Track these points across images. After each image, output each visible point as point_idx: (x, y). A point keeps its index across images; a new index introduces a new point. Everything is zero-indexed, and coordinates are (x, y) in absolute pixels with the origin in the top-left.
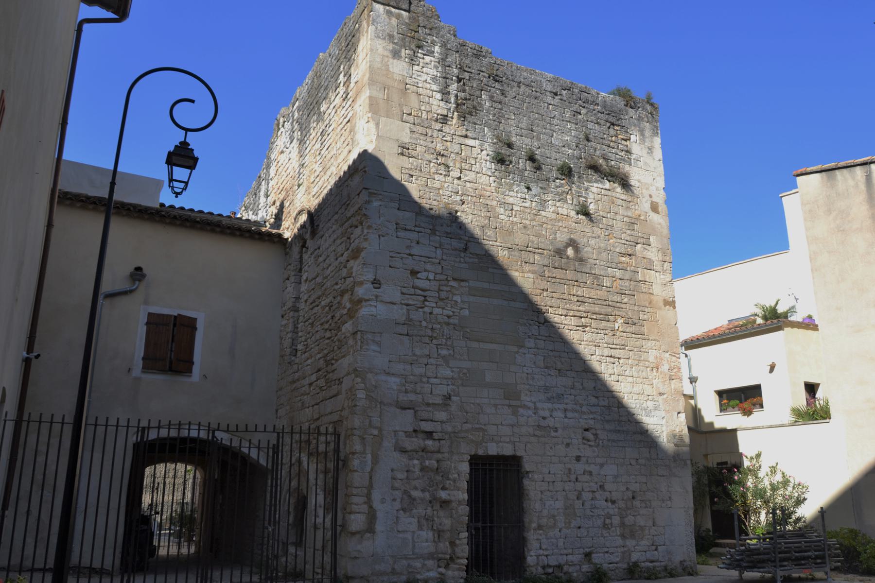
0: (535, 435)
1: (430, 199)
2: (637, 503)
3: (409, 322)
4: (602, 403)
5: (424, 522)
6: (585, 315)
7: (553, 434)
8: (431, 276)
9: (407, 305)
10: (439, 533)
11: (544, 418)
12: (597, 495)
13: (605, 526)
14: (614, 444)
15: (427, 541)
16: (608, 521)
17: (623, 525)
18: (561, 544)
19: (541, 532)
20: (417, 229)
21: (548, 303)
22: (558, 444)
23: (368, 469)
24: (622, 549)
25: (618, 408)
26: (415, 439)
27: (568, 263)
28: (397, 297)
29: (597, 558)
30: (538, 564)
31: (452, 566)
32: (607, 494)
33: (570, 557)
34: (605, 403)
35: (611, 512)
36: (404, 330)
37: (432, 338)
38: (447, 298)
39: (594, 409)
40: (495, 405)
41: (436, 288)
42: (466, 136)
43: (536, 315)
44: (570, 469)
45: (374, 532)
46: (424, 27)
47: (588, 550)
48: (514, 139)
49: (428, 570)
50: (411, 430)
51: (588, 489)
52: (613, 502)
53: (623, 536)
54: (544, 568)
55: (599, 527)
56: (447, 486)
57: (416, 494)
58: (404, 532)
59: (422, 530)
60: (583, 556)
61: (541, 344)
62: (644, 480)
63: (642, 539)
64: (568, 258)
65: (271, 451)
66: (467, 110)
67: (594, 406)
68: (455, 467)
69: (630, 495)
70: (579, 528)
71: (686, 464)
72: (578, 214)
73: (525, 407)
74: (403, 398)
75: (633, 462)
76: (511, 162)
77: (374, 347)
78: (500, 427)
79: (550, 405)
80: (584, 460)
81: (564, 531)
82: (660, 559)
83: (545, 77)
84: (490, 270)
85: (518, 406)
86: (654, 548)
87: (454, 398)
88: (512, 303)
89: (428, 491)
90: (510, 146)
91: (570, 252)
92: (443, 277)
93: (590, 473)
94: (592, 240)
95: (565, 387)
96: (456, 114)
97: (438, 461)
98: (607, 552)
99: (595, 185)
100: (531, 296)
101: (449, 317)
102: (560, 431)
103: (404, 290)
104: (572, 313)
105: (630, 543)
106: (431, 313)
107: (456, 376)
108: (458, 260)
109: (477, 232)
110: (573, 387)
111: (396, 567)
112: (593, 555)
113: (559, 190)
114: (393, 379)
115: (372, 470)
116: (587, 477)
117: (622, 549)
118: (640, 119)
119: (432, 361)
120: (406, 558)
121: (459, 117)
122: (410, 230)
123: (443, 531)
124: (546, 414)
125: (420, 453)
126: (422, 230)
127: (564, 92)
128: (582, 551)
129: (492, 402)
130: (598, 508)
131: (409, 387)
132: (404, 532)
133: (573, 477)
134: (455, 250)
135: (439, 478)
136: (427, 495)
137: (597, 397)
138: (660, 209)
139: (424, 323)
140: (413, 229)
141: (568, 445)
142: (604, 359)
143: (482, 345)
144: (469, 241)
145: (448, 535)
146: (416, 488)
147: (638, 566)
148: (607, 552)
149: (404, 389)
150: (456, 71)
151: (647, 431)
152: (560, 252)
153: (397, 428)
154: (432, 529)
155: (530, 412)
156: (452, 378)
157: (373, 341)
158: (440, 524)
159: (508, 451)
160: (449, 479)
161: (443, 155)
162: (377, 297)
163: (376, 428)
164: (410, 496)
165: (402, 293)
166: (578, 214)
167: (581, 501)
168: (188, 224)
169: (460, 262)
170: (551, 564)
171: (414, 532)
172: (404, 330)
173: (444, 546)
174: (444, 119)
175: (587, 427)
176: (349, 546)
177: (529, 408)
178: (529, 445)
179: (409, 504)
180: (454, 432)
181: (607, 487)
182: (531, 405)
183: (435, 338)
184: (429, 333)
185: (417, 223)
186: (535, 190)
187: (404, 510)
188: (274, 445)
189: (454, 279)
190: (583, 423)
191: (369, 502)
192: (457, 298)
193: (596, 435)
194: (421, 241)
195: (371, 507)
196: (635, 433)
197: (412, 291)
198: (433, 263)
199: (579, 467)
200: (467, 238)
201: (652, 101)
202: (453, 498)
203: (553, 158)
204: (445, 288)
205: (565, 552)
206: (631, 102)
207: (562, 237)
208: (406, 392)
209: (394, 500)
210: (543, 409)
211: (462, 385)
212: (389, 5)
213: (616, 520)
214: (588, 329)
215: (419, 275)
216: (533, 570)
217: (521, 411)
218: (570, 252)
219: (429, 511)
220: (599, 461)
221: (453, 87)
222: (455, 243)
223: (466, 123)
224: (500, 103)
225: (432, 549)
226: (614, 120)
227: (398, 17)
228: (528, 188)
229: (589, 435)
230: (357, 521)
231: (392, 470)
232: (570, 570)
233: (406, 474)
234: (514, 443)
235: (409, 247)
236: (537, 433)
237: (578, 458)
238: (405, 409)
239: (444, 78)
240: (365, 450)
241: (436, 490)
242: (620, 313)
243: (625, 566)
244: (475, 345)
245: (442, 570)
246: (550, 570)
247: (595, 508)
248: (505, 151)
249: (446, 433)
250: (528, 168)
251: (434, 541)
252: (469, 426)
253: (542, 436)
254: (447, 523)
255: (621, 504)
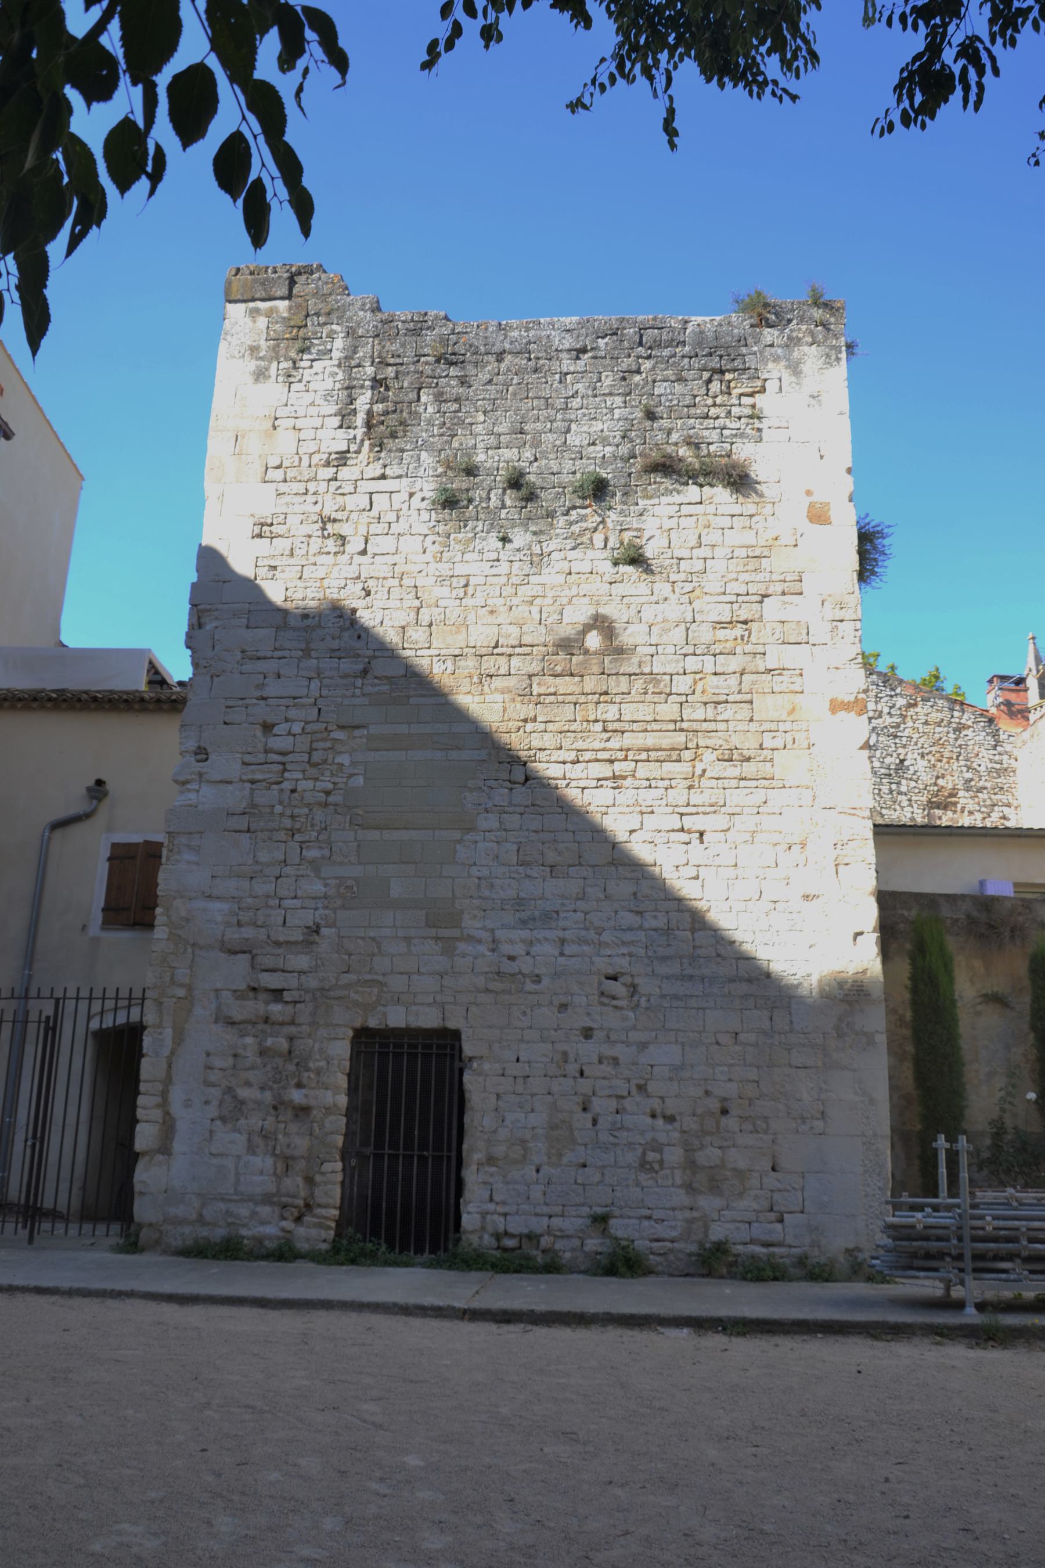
0: (487, 990)
1: (304, 599)
2: (730, 1122)
3: (251, 810)
4: (650, 922)
5: (258, 1140)
6: (620, 755)
7: (530, 986)
8: (297, 728)
9: (253, 782)
10: (287, 1162)
11: (512, 958)
12: (627, 1103)
13: (644, 1165)
14: (675, 1003)
15: (261, 1173)
16: (651, 1156)
17: (691, 1165)
18: (537, 1192)
19: (493, 1169)
20: (277, 654)
21: (536, 744)
22: (539, 1005)
23: (166, 1052)
24: (688, 1214)
25: (693, 930)
26: (251, 1003)
27: (585, 662)
28: (234, 769)
29: (619, 1228)
30: (483, 1228)
31: (307, 1219)
32: (655, 1104)
33: (557, 1222)
34: (661, 922)
35: (662, 1138)
36: (243, 823)
37: (293, 832)
38: (325, 761)
39: (628, 937)
40: (408, 939)
41: (306, 747)
42: (383, 477)
43: (511, 769)
44: (565, 1054)
45: (170, 1154)
46: (317, 314)
47: (599, 1210)
48: (480, 457)
49: (263, 1223)
50: (243, 987)
51: (607, 1092)
52: (670, 1119)
53: (689, 1188)
54: (498, 1237)
55: (629, 1167)
56: (305, 1081)
57: (244, 1093)
58: (222, 1155)
59: (254, 1154)
60: (588, 1221)
61: (513, 821)
62: (752, 1074)
63: (741, 1195)
64: (587, 652)
65: (43, 1025)
66: (385, 431)
67: (630, 929)
68: (321, 1050)
69: (714, 1105)
70: (585, 1166)
71: (871, 1042)
72: (616, 564)
73: (471, 939)
74: (234, 935)
75: (723, 1039)
76: (470, 501)
77: (188, 856)
78: (415, 977)
79: (525, 934)
80: (598, 1035)
81: (545, 1169)
82: (789, 1240)
83: (559, 327)
84: (412, 701)
85: (457, 939)
86: (772, 1216)
87: (324, 931)
88: (454, 754)
89: (271, 1089)
90: (471, 471)
91: (593, 640)
92: (321, 726)
93: (615, 1061)
94: (647, 612)
95: (563, 897)
96: (367, 443)
97: (291, 1039)
98: (649, 1218)
99: (664, 500)
100: (496, 735)
101: (328, 793)
102: (546, 981)
103: (248, 758)
104: (588, 756)
105: (707, 1203)
106: (293, 791)
107: (332, 892)
108: (349, 693)
109: (392, 637)
110: (583, 897)
111: (205, 1213)
112: (612, 1222)
113: (576, 528)
114: (218, 905)
115: (172, 1053)
116: (607, 1069)
117: (688, 1214)
118: (793, 342)
119: (288, 870)
120: (223, 1200)
121: (372, 446)
122: (265, 658)
123: (293, 1158)
124: (519, 949)
125: (260, 1027)
126: (286, 653)
127: (601, 342)
128: (585, 1210)
129: (401, 933)
130: (628, 1130)
131: (244, 917)
132: (222, 1155)
133: (572, 1068)
134: (346, 676)
135: (291, 1067)
136: (268, 1097)
137: (640, 913)
138: (833, 514)
139: (278, 809)
140: (269, 654)
141: (563, 1007)
142: (659, 839)
143: (387, 835)
144: (375, 657)
145: (302, 1164)
146: (248, 1084)
147: (726, 1252)
148: (649, 1218)
149: (234, 920)
150: (370, 370)
151: (768, 975)
152: (567, 646)
153: (219, 985)
154: (274, 1154)
155: (482, 949)
156: (325, 897)
157: (188, 846)
158: (288, 1146)
159: (428, 1019)
160: (308, 1070)
161: (335, 521)
162: (201, 775)
163: (182, 985)
164: (235, 1097)
165: (244, 763)
166: (616, 564)
167: (589, 1116)
168: (19, 705)
169: (354, 696)
170: (511, 1230)
171: (239, 1157)
172: (243, 823)
173: (294, 1183)
174: (342, 458)
175: (611, 971)
176: (144, 1176)
177: (480, 941)
178: (473, 1009)
179: (233, 1110)
180: (323, 989)
181: (651, 1087)
182: (485, 935)
183: (299, 831)
184: (288, 823)
185: (277, 645)
186: (520, 538)
187: (223, 1119)
188: (48, 1018)
189: (341, 727)
190: (602, 964)
191: (164, 1103)
192: (345, 759)
193: (633, 988)
194: (282, 672)
195: (167, 1113)
196: (732, 980)
197: (261, 757)
198: (303, 706)
199: (589, 1050)
200: (370, 653)
201: (827, 297)
202: (312, 1103)
203: (560, 470)
204: (321, 745)
205: (546, 1210)
206: (765, 314)
207: (578, 614)
208: (239, 924)
209: (207, 1102)
210: (511, 942)
211: (343, 907)
212: (253, 300)
213: (674, 1155)
214: (628, 782)
215: (276, 730)
216: (474, 1239)
217: (462, 946)
218: (593, 640)
219: (269, 1123)
220: (635, 1036)
221: (363, 401)
222: (346, 666)
223: (383, 455)
224: (457, 400)
225: (272, 1188)
226: (723, 361)
227: (269, 313)
228: (505, 540)
229: (617, 988)
230: (145, 1136)
231: (208, 1054)
232: (557, 1247)
233: (231, 1061)
234: (443, 1006)
235: (260, 686)
236: (492, 986)
237: (587, 1033)
238: (235, 953)
239: (347, 388)
240: (161, 1020)
241: (284, 1088)
242: (710, 742)
243: (693, 1248)
244: (374, 835)
245: (288, 1225)
246: (510, 1243)
247: (622, 1128)
248: (460, 483)
249: (307, 991)
250: (508, 503)
251: (275, 1174)
252: (352, 977)
253: (503, 992)
254: (301, 1144)
255: (690, 1123)
